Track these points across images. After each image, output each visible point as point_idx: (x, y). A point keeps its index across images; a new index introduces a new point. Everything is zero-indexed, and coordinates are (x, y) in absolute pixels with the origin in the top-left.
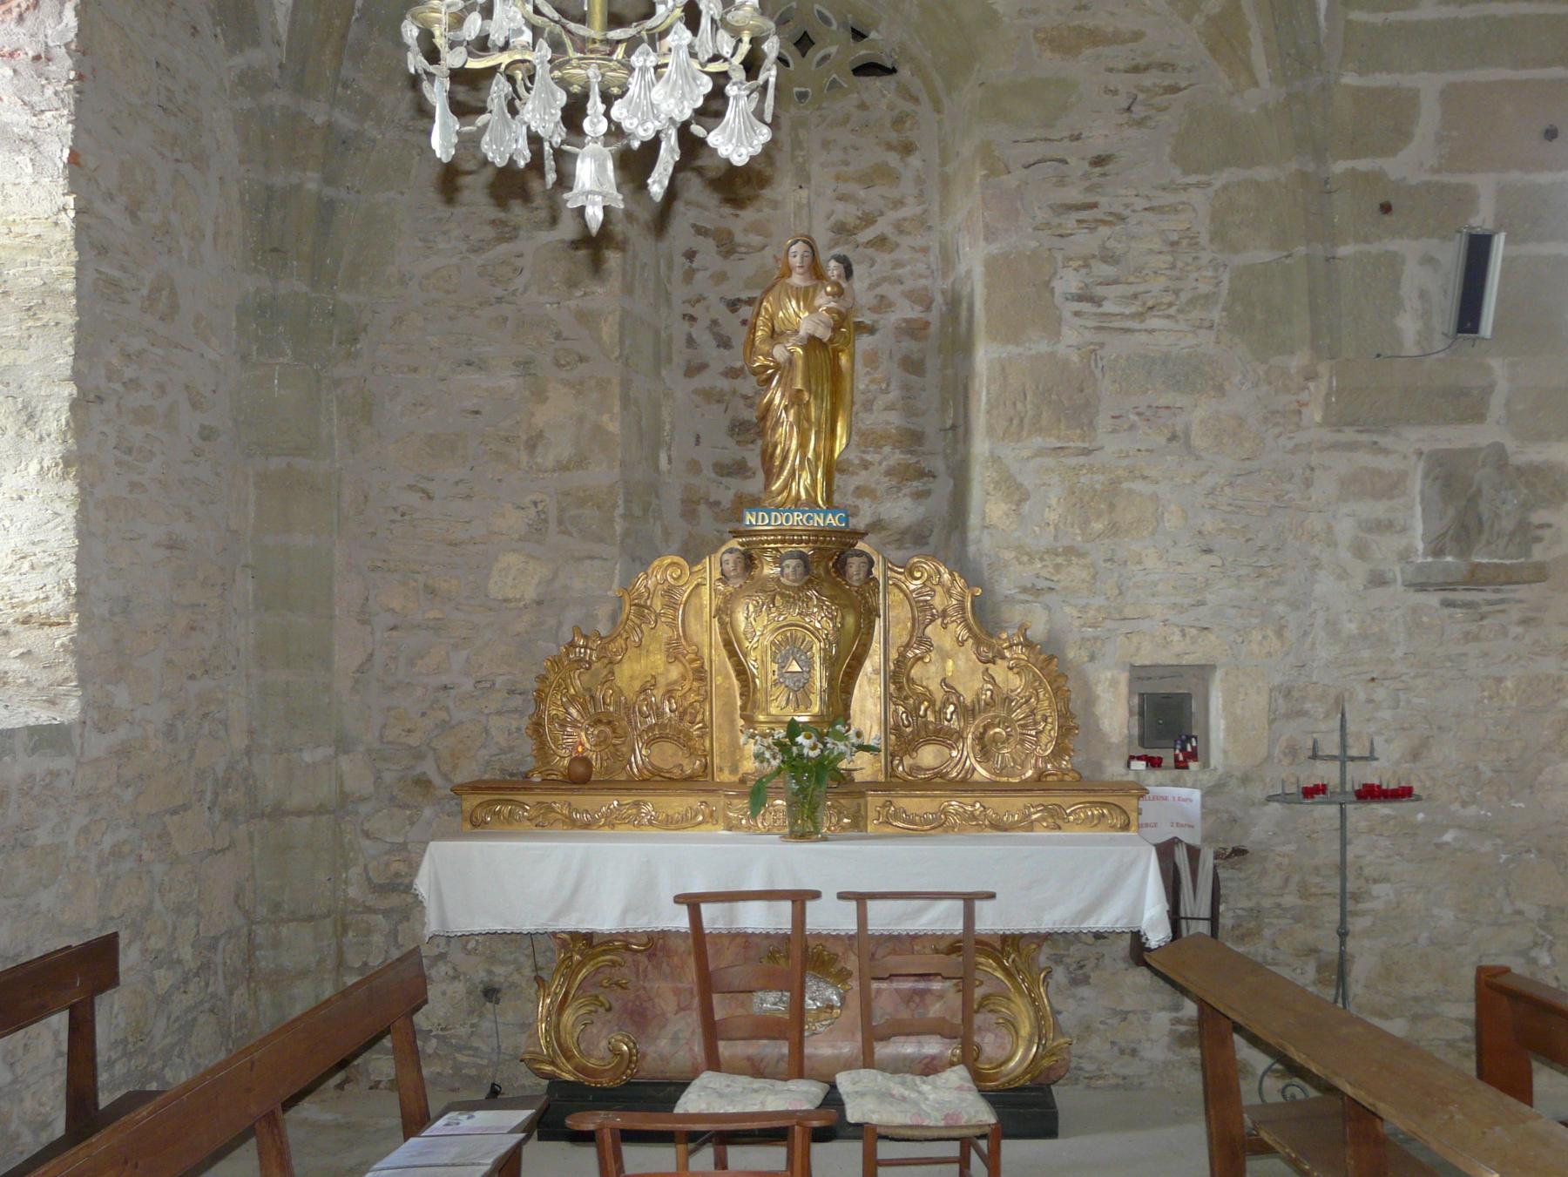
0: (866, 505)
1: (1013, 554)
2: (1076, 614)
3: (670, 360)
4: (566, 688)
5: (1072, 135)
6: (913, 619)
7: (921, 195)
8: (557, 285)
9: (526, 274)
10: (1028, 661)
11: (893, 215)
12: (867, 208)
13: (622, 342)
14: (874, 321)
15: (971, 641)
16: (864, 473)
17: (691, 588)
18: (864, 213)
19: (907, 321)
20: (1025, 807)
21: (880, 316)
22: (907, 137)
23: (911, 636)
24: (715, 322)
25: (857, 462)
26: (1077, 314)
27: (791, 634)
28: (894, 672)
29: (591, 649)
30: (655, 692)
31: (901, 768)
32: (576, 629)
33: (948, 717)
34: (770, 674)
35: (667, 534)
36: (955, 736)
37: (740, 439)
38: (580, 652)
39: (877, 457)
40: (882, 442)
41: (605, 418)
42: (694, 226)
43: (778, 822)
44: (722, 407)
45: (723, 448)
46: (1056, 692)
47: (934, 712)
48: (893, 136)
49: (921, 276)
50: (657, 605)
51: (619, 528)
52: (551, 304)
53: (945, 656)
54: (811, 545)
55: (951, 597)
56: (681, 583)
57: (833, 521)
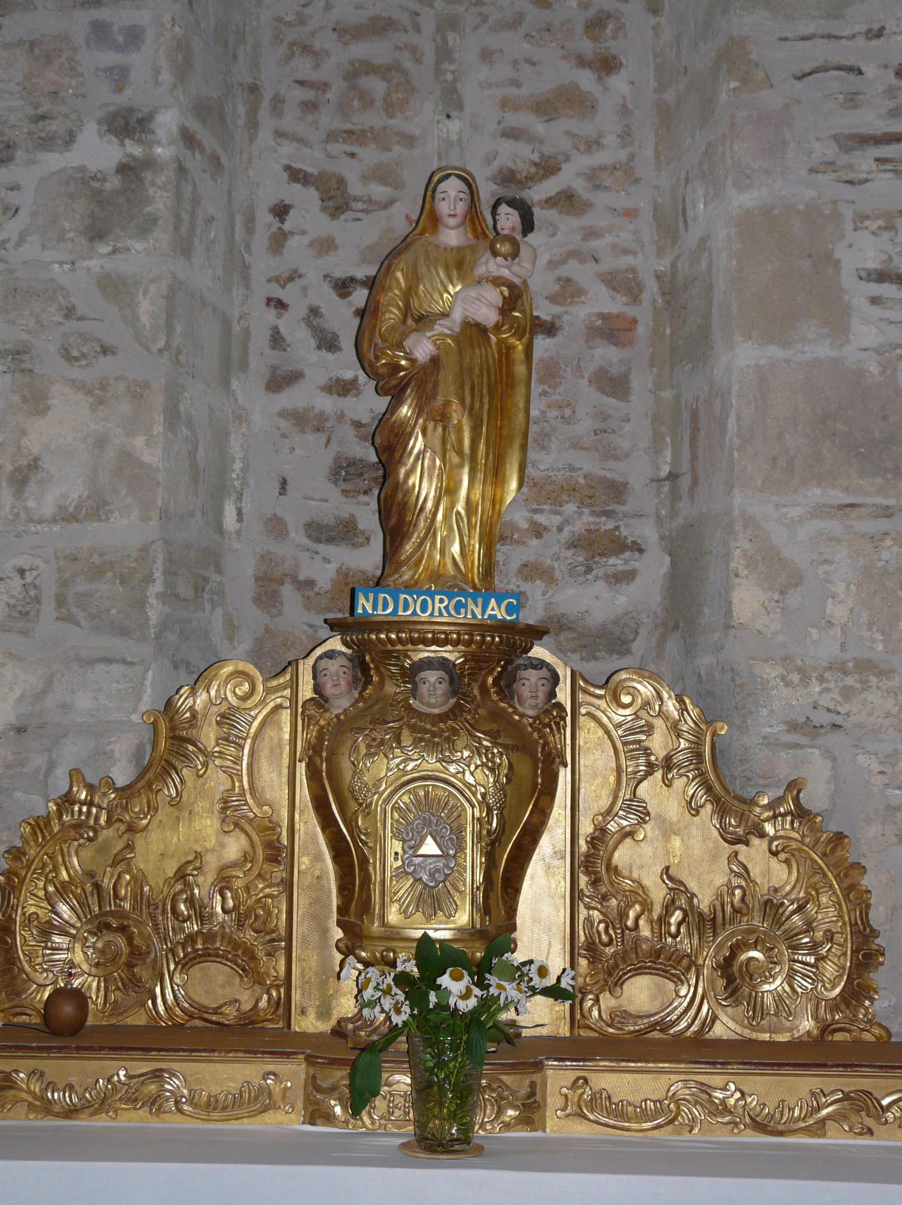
0: (538, 592)
1: (779, 670)
2: (876, 767)
3: (244, 366)
4: (56, 869)
5: (870, 31)
6: (619, 770)
7: (626, 136)
8: (71, 235)
9: (23, 217)
10: (802, 842)
11: (583, 161)
12: (547, 149)
13: (169, 329)
14: (554, 317)
15: (709, 807)
16: (535, 542)
17: (265, 712)
18: (542, 156)
19: (604, 317)
20: (813, 1094)
21: (563, 309)
22: (607, 48)
23: (616, 798)
24: (314, 311)
25: (524, 525)
26: (875, 301)
27: (427, 793)
28: (588, 856)
29: (100, 807)
30: (201, 879)
31: (595, 1013)
32: (75, 774)
33: (673, 929)
34: (390, 858)
35: (231, 629)
36: (685, 962)
37: (344, 487)
38: (80, 811)
39: (557, 519)
40: (565, 497)
41: (139, 441)
42: (288, 168)
43: (397, 1113)
44: (323, 438)
45: (321, 500)
46: (849, 890)
47: (651, 922)
48: (587, 47)
49: (626, 252)
50: (209, 735)
51: (155, 612)
52: (61, 263)
53: (668, 830)
54: (461, 648)
55: (679, 736)
56: (249, 703)
57: (497, 611)
